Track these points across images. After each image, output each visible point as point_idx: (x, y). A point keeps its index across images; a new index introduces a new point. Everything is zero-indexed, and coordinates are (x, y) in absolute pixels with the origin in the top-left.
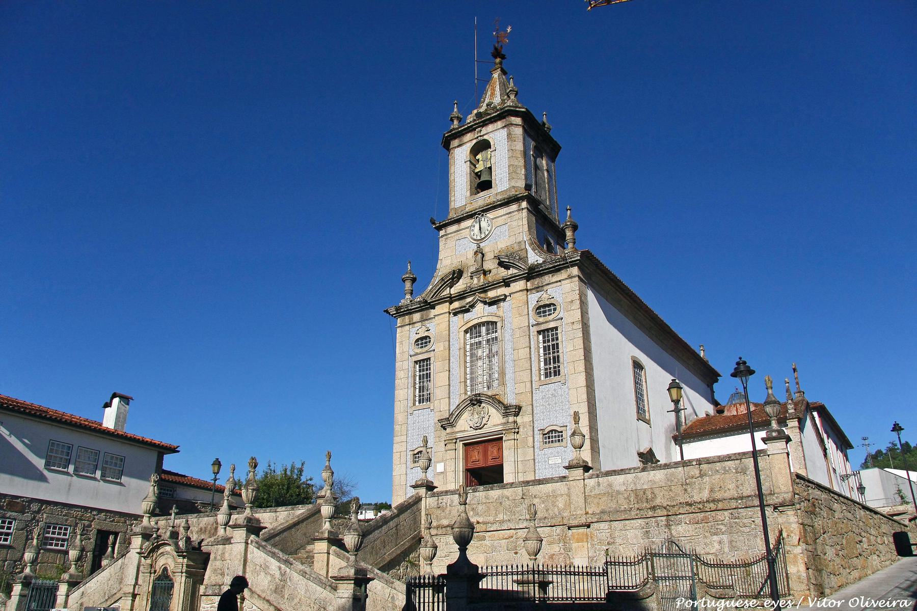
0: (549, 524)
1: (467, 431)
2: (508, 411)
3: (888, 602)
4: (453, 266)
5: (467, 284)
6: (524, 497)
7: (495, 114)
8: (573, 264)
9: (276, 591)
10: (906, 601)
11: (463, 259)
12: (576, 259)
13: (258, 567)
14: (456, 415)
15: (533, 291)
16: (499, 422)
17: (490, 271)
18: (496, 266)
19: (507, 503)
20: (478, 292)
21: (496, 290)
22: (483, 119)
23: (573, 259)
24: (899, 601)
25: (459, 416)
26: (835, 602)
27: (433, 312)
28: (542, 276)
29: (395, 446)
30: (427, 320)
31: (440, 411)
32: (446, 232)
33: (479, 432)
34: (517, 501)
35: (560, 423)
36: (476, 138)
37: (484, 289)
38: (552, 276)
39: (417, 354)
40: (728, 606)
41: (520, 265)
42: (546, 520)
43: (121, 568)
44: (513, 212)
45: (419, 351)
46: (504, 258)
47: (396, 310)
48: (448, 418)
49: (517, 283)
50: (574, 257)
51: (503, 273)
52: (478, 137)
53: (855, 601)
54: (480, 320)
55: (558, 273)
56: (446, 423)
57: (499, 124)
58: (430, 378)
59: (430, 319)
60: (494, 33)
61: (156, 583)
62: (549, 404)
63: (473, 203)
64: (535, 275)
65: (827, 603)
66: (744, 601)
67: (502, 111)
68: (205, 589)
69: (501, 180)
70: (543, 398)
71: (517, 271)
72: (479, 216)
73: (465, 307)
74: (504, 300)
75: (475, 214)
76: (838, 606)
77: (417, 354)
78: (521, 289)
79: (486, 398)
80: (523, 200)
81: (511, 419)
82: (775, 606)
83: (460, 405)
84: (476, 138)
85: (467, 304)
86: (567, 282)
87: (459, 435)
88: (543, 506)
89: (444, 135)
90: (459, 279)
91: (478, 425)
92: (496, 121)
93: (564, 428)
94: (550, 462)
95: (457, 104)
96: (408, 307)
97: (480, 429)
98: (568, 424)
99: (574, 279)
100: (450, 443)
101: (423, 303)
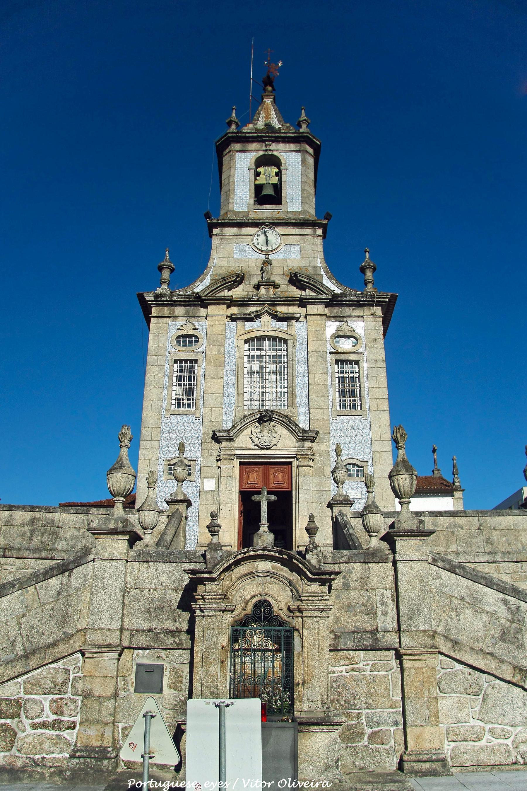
0: (515, 560)
1: (250, 449)
2: (306, 435)
4: (231, 269)
5: (248, 292)
6: (482, 528)
7: (291, 135)
8: (378, 304)
9: (503, 638)
11: (244, 266)
12: (384, 300)
13: (456, 602)
14: (238, 429)
15: (332, 319)
16: (292, 446)
17: (279, 286)
18: (286, 282)
19: (461, 533)
20: (267, 304)
21: (287, 307)
22: (277, 135)
25: (240, 431)
27: (202, 312)
28: (342, 307)
29: (142, 451)
30: (195, 317)
32: (222, 231)
33: (265, 452)
34: (473, 532)
35: (361, 458)
36: (263, 150)
37: (274, 302)
38: (353, 309)
39: (179, 352)
41: (322, 289)
42: (511, 556)
43: (58, 594)
44: (307, 235)
45: (181, 349)
46: (303, 277)
47: (154, 297)
48: (229, 431)
49: (316, 306)
50: (382, 298)
51: (295, 292)
52: (266, 150)
54: (266, 333)
55: (360, 308)
57: (292, 146)
58: (194, 381)
59: (199, 317)
60: (266, 63)
61: (237, 630)
62: (348, 436)
63: (258, 213)
67: (300, 135)
68: (334, 639)
69: (293, 199)
70: (341, 429)
71: (315, 294)
72: (266, 228)
73: (250, 314)
74: (297, 319)
75: (263, 224)
77: (179, 352)
78: (320, 313)
79: (280, 416)
80: (319, 228)
81: (307, 444)
84: (263, 150)
85: (253, 312)
86: (370, 320)
87: (238, 452)
88: (504, 539)
89: (228, 134)
90: (239, 284)
93: (365, 463)
95: (235, 109)
96: (172, 297)
98: (369, 460)
99: (377, 319)
100: (226, 459)
101: (194, 298)
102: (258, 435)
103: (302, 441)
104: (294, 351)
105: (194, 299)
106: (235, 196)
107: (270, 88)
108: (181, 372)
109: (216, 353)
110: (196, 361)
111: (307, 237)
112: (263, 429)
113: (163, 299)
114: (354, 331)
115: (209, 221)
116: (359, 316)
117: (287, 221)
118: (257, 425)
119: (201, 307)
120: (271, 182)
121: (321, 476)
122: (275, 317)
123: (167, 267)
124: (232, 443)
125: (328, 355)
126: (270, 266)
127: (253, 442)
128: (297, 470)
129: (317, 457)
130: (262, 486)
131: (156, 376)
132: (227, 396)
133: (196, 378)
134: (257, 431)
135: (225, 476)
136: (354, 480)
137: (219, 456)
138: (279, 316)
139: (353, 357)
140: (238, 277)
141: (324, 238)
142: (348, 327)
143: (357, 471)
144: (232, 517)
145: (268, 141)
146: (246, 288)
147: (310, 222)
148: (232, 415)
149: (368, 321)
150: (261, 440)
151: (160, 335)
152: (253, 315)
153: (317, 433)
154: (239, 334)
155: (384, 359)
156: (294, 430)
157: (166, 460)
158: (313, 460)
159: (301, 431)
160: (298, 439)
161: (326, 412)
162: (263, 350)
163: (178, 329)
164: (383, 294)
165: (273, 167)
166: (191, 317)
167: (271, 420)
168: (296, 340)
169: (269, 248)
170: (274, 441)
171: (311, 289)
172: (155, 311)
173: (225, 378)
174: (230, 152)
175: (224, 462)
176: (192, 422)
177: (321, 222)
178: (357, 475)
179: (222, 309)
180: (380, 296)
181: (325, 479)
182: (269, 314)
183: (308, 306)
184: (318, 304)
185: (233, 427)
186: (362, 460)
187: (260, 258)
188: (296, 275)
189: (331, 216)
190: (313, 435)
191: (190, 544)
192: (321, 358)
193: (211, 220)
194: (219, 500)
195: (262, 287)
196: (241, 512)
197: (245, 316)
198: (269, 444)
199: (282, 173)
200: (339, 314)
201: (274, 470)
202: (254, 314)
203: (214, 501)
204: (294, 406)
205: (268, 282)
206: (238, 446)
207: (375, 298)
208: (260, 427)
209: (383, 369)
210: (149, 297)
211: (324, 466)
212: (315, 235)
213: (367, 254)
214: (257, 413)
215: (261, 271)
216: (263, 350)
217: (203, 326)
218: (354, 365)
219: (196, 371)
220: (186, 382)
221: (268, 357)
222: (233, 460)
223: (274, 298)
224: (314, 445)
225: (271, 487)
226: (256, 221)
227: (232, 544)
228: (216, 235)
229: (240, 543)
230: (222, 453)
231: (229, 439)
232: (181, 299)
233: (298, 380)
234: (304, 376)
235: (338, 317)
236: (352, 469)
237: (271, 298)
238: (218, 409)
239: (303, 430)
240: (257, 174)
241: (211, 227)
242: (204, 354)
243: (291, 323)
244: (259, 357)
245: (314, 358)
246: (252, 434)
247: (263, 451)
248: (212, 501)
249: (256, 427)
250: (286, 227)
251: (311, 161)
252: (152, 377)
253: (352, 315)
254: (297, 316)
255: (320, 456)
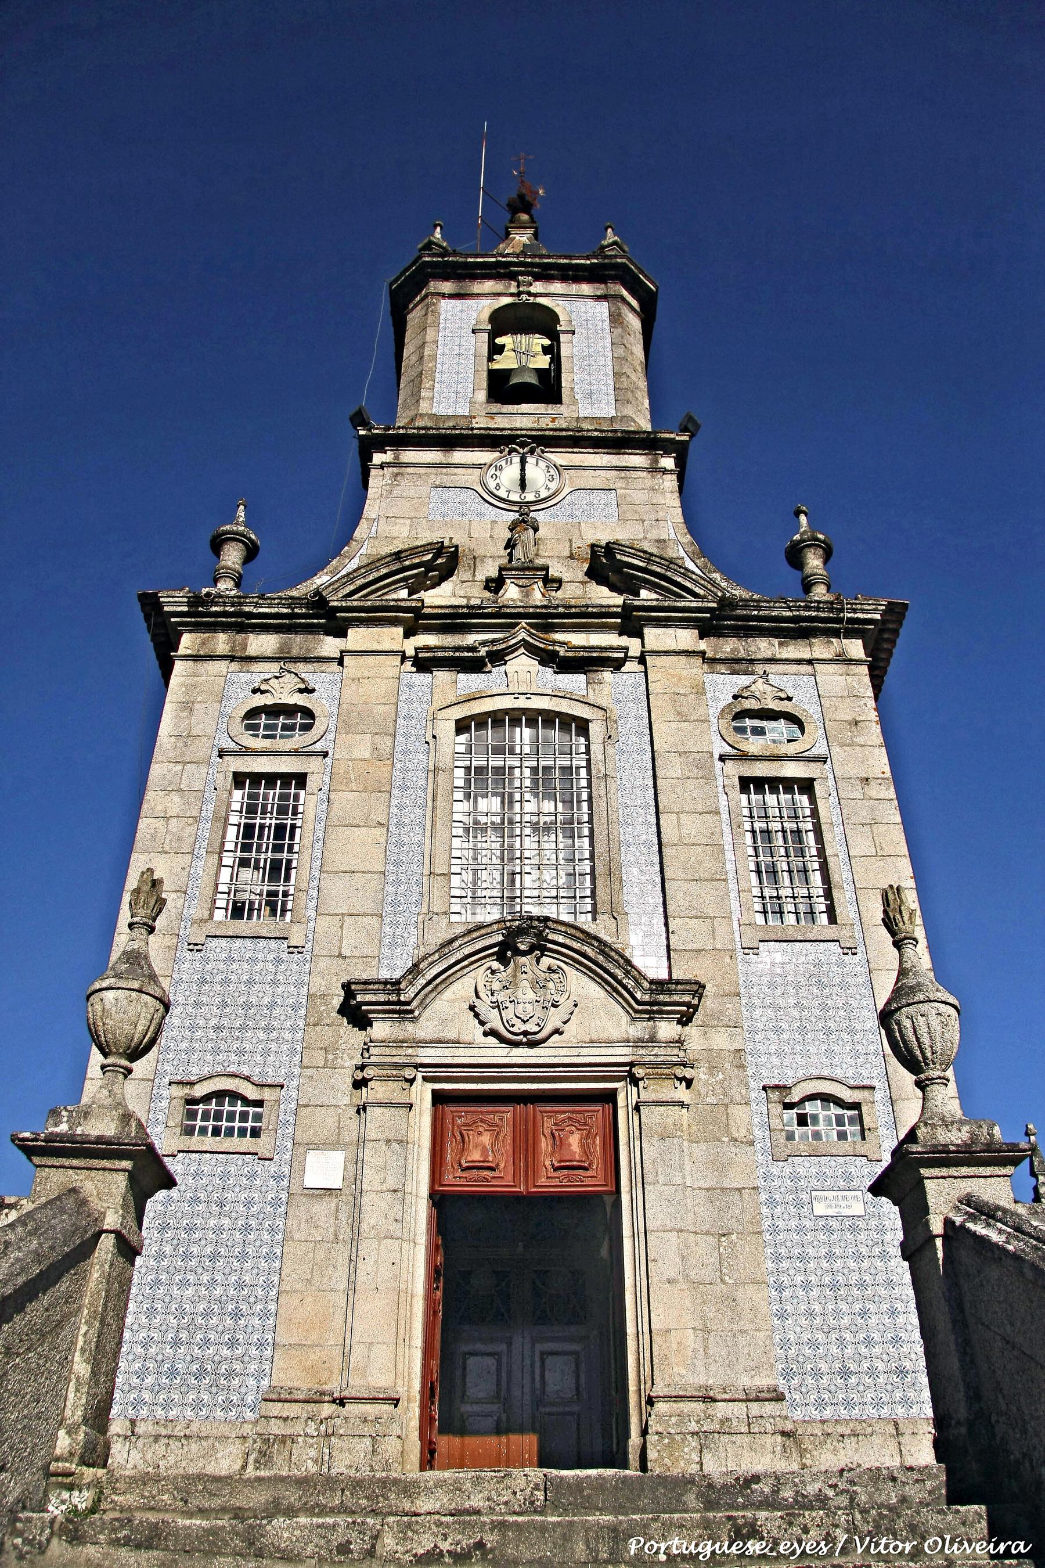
1: (470, 1045)
2: (661, 998)
3: (992, 1545)
7: (583, 262)
8: (854, 629)
10: (1022, 1543)
12: (869, 616)
15: (722, 668)
16: (616, 1034)
17: (559, 582)
18: (581, 576)
23: (860, 616)
24: (1010, 1543)
25: (439, 983)
26: (901, 1545)
27: (330, 645)
28: (747, 636)
30: (306, 660)
31: (340, 956)
36: (512, 295)
38: (781, 644)
40: (717, 1552)
41: (688, 584)
46: (632, 555)
47: (189, 604)
48: (398, 982)
49: (670, 631)
50: (863, 611)
53: (936, 1543)
54: (522, 703)
56: (382, 998)
59: (320, 660)
64: (727, 627)
65: (887, 1546)
66: (745, 1544)
69: (591, 394)
74: (617, 665)
76: (907, 1552)
79: (573, 937)
80: (667, 453)
81: (667, 1029)
82: (799, 1552)
83: (456, 944)
87: (429, 1055)
91: (531, 1027)
92: (577, 280)
93: (866, 1093)
94: (820, 1209)
96: (241, 604)
97: (532, 1044)
98: (875, 1083)
100: (386, 1078)
102: (501, 997)
103: (649, 1019)
104: (610, 750)
105: (307, 608)
106: (436, 385)
107: (525, 217)
108: (251, 810)
109: (367, 756)
110: (301, 780)
111: (633, 474)
112: (515, 976)
113: (214, 609)
114: (789, 699)
115: (362, 433)
116: (799, 662)
117: (577, 434)
118: (496, 965)
119: (328, 634)
120: (531, 366)
121: (719, 1140)
122: (547, 658)
123: (236, 537)
124: (410, 1027)
125: (719, 764)
126: (531, 531)
127: (482, 1023)
128: (636, 1118)
129: (700, 1074)
130: (510, 1177)
131: (173, 822)
132: (397, 882)
133: (298, 831)
134: (496, 986)
135: (380, 1137)
136: (834, 1152)
137: (362, 1068)
138: (561, 654)
139: (792, 770)
140: (438, 554)
141: (681, 479)
142: (770, 688)
143: (840, 1120)
144: (403, 1286)
145: (522, 274)
146: (461, 588)
147: (642, 436)
148: (412, 940)
149: (828, 674)
150: (508, 1014)
151: (197, 706)
152: (483, 651)
153: (698, 989)
154: (439, 702)
155: (888, 774)
156: (620, 983)
157: (180, 1083)
158: (689, 1083)
159: (646, 985)
160: (636, 1011)
161: (721, 928)
162: (512, 752)
163: (255, 691)
164: (865, 599)
165: (537, 336)
166: (296, 660)
167: (543, 949)
168: (616, 722)
169: (530, 497)
170: (555, 1017)
171: (653, 587)
172: (187, 642)
173: (393, 829)
174: (426, 296)
175: (378, 1091)
176: (279, 961)
177: (672, 436)
178: (842, 1136)
179: (391, 637)
180: (859, 607)
181: (733, 1149)
182: (532, 650)
183: (646, 630)
184: (677, 626)
185: (415, 970)
186: (852, 1083)
187: (505, 518)
188: (609, 549)
189: (697, 426)
190: (687, 998)
191: (243, 1390)
192: (695, 771)
193: (369, 430)
194: (356, 1224)
195: (508, 581)
196: (437, 1271)
197: (457, 654)
198: (537, 1029)
199: (562, 340)
200: (742, 654)
201: (553, 1121)
202: (487, 649)
203: (338, 1228)
204: (616, 914)
205: (528, 569)
206: (429, 1037)
207: (842, 610)
208: (505, 974)
209: (889, 803)
210: (174, 602)
211: (726, 1106)
212: (655, 470)
213: (803, 519)
214: (495, 927)
215: (506, 548)
216: (512, 752)
217: (332, 682)
218: (797, 796)
219: (300, 809)
220: (268, 839)
221: (527, 772)
222: (411, 1081)
223: (545, 607)
224: (692, 1031)
225: (542, 1181)
226: (491, 432)
227: (401, 1391)
228: (382, 466)
229: (432, 1389)
230: (373, 1059)
231: (399, 1012)
232: (267, 610)
233: (625, 833)
234: (646, 823)
235: (738, 661)
236: (822, 1114)
237: (537, 607)
238: (366, 920)
239: (652, 982)
240: (496, 350)
241: (368, 447)
242: (328, 760)
243: (598, 676)
244: (499, 770)
245: (671, 769)
246: (477, 996)
247: (516, 1051)
248: (332, 1230)
249: (493, 972)
250: (575, 450)
251: (634, 323)
252: (160, 824)
253: (778, 656)
254: (616, 655)
255: (712, 1070)
